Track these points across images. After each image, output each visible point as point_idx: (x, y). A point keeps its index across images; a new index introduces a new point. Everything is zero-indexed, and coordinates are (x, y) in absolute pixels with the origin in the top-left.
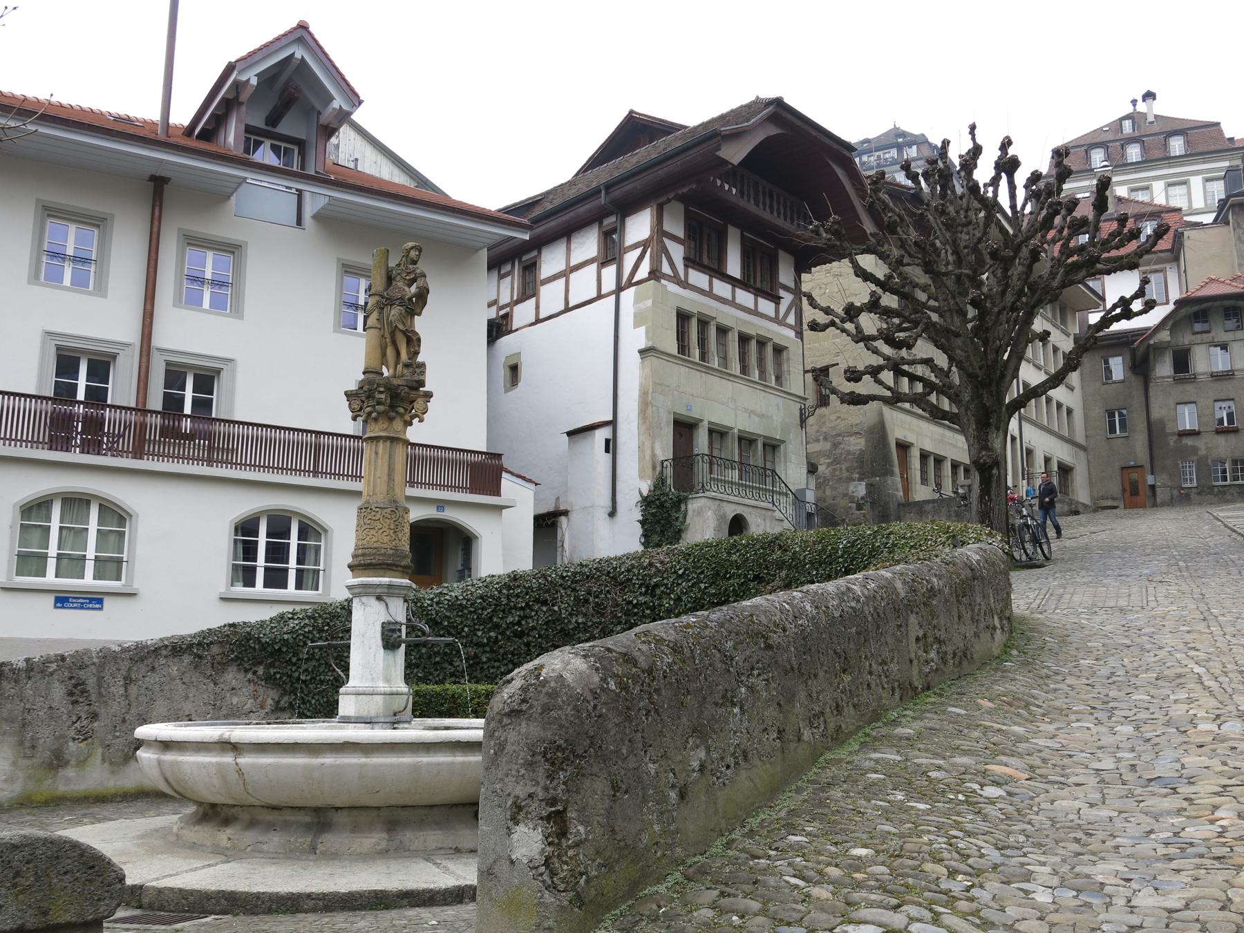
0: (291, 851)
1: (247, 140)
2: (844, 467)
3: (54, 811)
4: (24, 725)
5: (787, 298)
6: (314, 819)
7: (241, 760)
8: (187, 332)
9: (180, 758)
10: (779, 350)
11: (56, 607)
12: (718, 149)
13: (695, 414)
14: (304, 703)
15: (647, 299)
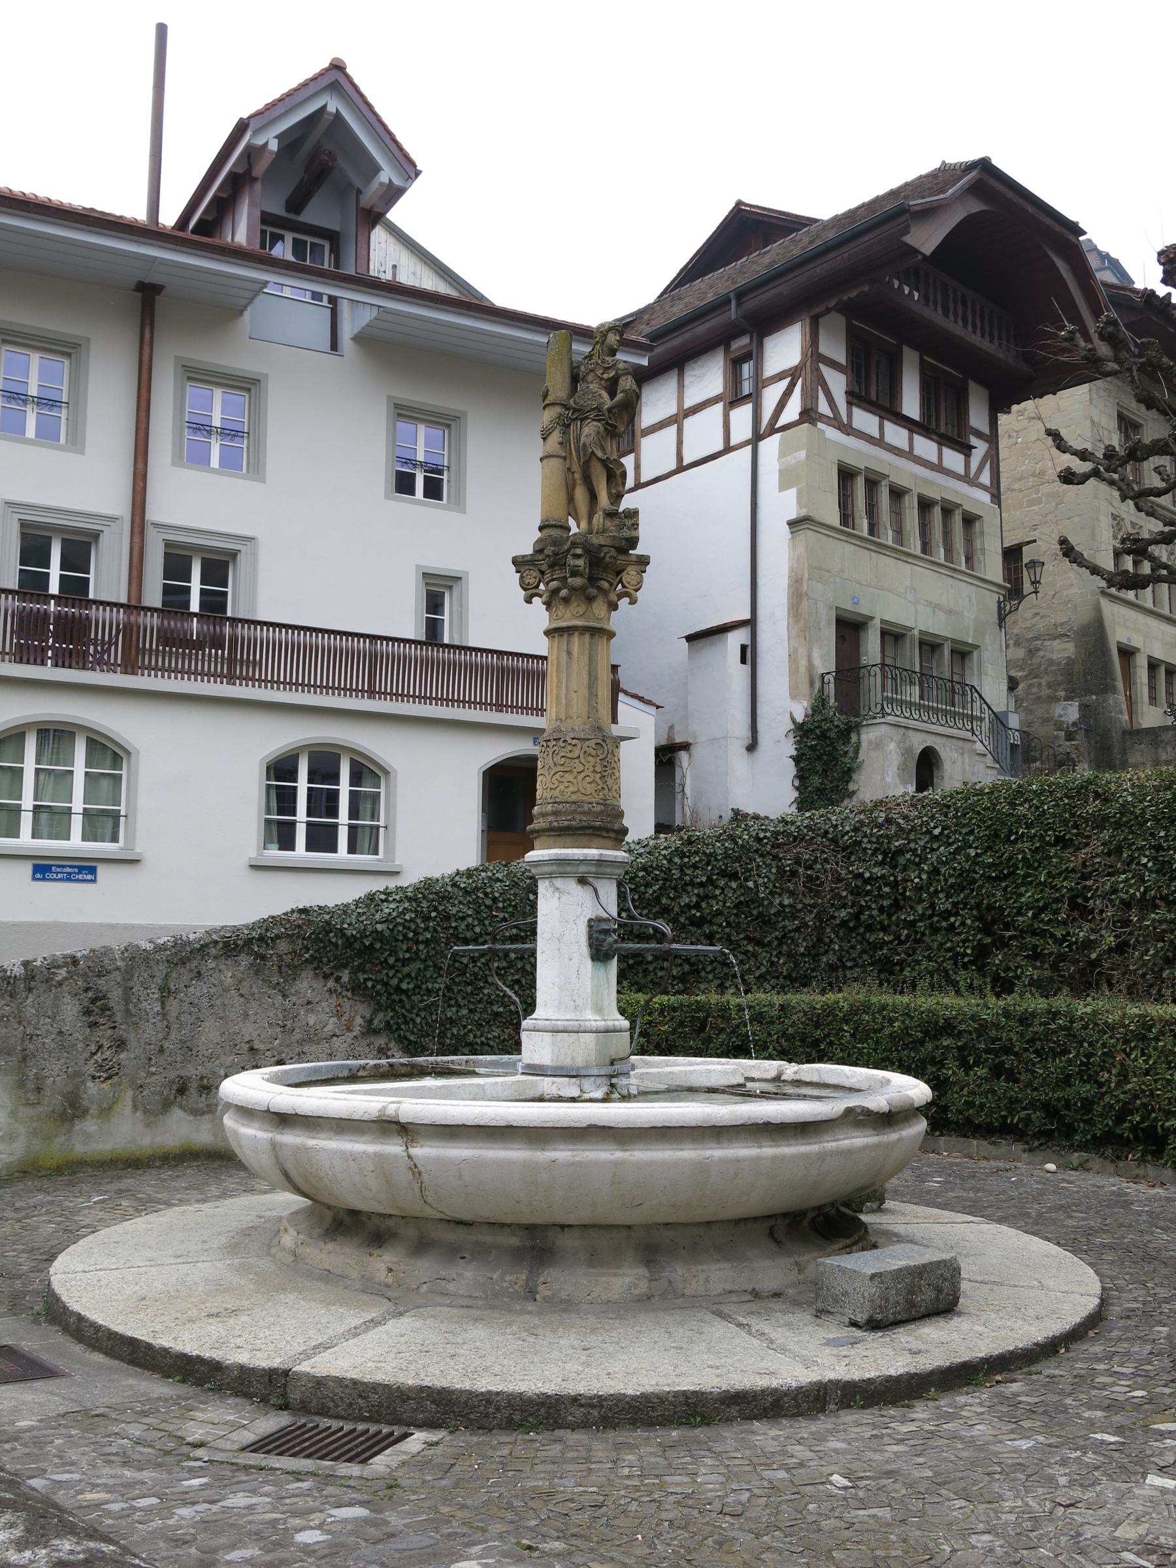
0: (495, 1295)
1: (263, 232)
3: (71, 1184)
4: (24, 1058)
5: (980, 448)
6: (524, 1246)
7: (418, 1151)
8: (193, 501)
9: (311, 1142)
10: (970, 520)
11: (34, 879)
12: (906, 231)
13: (864, 610)
14: (406, 1023)
15: (797, 449)
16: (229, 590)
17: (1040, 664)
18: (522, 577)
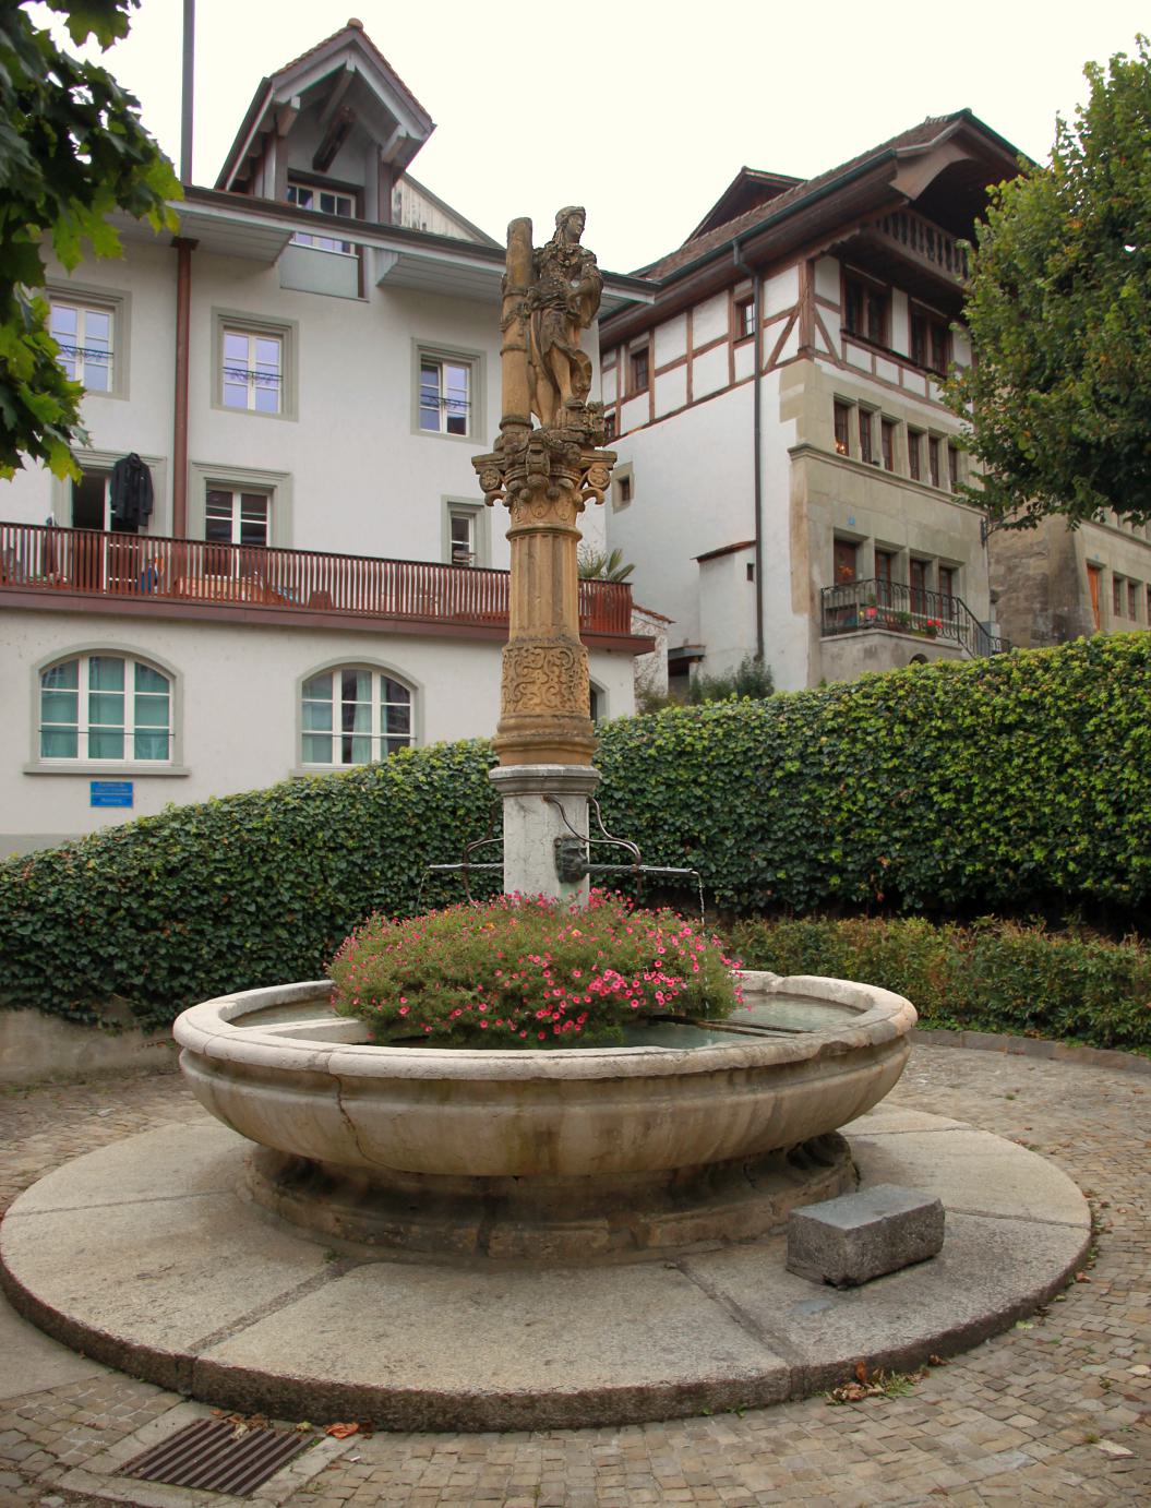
2: (1021, 595)
7: (351, 1105)
8: (230, 442)
12: (893, 175)
16: (268, 523)
17: (1019, 579)
18: (481, 478)
